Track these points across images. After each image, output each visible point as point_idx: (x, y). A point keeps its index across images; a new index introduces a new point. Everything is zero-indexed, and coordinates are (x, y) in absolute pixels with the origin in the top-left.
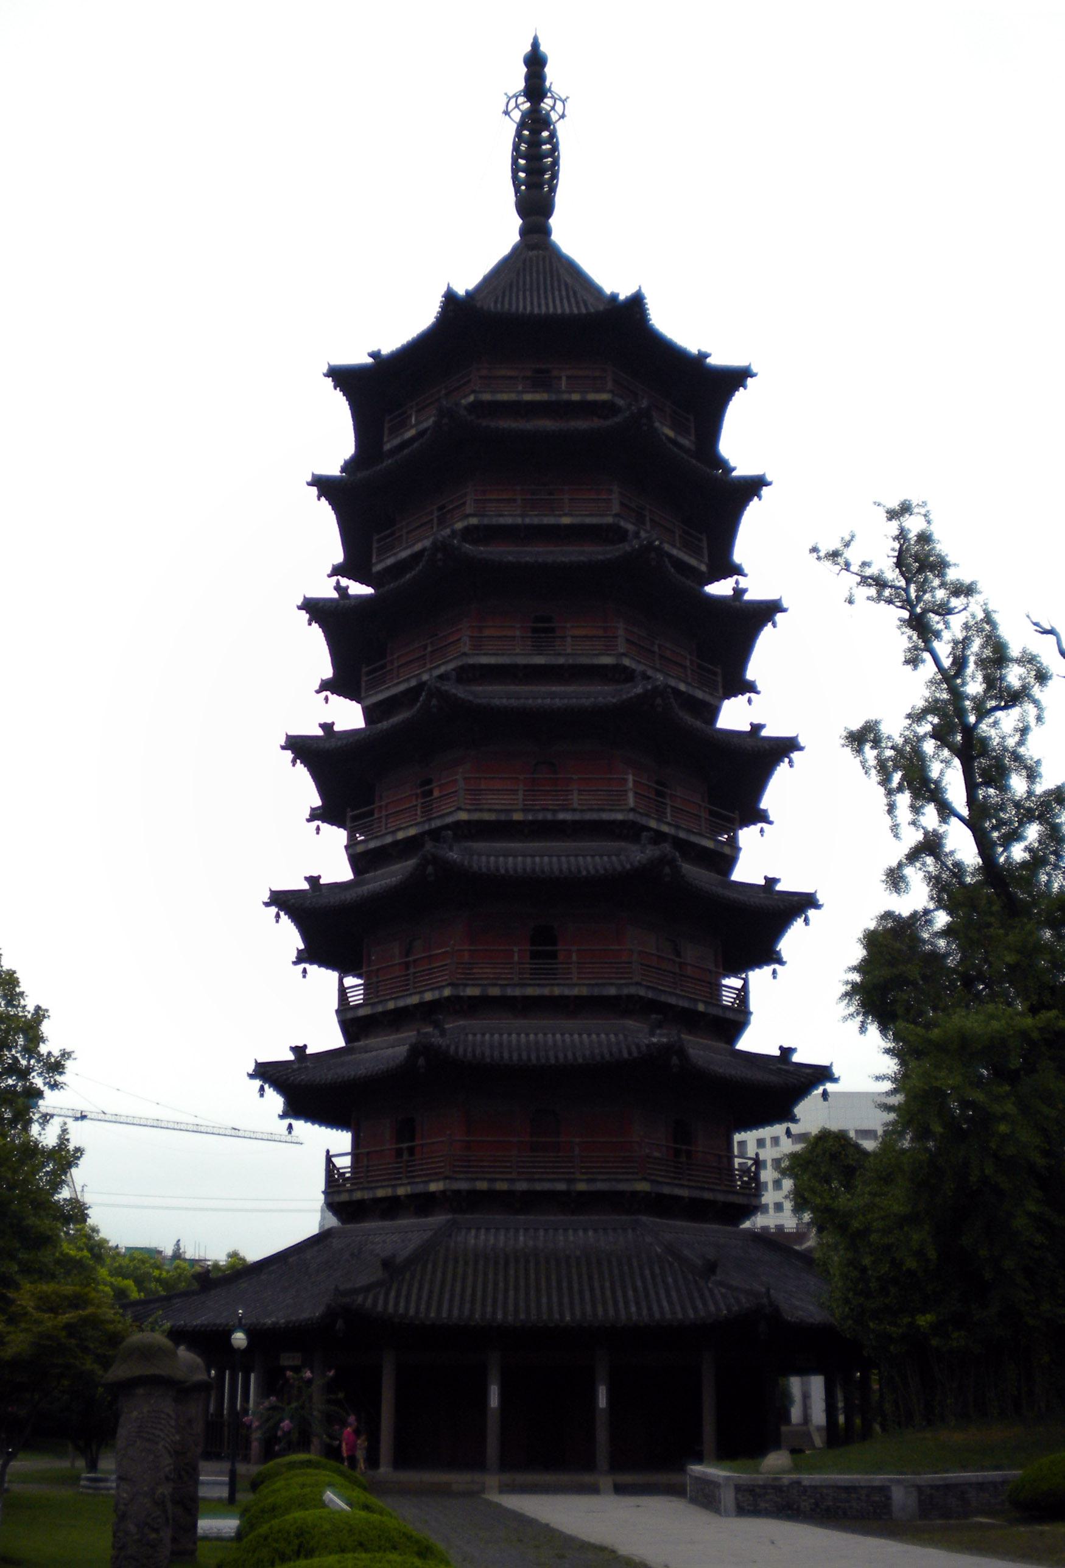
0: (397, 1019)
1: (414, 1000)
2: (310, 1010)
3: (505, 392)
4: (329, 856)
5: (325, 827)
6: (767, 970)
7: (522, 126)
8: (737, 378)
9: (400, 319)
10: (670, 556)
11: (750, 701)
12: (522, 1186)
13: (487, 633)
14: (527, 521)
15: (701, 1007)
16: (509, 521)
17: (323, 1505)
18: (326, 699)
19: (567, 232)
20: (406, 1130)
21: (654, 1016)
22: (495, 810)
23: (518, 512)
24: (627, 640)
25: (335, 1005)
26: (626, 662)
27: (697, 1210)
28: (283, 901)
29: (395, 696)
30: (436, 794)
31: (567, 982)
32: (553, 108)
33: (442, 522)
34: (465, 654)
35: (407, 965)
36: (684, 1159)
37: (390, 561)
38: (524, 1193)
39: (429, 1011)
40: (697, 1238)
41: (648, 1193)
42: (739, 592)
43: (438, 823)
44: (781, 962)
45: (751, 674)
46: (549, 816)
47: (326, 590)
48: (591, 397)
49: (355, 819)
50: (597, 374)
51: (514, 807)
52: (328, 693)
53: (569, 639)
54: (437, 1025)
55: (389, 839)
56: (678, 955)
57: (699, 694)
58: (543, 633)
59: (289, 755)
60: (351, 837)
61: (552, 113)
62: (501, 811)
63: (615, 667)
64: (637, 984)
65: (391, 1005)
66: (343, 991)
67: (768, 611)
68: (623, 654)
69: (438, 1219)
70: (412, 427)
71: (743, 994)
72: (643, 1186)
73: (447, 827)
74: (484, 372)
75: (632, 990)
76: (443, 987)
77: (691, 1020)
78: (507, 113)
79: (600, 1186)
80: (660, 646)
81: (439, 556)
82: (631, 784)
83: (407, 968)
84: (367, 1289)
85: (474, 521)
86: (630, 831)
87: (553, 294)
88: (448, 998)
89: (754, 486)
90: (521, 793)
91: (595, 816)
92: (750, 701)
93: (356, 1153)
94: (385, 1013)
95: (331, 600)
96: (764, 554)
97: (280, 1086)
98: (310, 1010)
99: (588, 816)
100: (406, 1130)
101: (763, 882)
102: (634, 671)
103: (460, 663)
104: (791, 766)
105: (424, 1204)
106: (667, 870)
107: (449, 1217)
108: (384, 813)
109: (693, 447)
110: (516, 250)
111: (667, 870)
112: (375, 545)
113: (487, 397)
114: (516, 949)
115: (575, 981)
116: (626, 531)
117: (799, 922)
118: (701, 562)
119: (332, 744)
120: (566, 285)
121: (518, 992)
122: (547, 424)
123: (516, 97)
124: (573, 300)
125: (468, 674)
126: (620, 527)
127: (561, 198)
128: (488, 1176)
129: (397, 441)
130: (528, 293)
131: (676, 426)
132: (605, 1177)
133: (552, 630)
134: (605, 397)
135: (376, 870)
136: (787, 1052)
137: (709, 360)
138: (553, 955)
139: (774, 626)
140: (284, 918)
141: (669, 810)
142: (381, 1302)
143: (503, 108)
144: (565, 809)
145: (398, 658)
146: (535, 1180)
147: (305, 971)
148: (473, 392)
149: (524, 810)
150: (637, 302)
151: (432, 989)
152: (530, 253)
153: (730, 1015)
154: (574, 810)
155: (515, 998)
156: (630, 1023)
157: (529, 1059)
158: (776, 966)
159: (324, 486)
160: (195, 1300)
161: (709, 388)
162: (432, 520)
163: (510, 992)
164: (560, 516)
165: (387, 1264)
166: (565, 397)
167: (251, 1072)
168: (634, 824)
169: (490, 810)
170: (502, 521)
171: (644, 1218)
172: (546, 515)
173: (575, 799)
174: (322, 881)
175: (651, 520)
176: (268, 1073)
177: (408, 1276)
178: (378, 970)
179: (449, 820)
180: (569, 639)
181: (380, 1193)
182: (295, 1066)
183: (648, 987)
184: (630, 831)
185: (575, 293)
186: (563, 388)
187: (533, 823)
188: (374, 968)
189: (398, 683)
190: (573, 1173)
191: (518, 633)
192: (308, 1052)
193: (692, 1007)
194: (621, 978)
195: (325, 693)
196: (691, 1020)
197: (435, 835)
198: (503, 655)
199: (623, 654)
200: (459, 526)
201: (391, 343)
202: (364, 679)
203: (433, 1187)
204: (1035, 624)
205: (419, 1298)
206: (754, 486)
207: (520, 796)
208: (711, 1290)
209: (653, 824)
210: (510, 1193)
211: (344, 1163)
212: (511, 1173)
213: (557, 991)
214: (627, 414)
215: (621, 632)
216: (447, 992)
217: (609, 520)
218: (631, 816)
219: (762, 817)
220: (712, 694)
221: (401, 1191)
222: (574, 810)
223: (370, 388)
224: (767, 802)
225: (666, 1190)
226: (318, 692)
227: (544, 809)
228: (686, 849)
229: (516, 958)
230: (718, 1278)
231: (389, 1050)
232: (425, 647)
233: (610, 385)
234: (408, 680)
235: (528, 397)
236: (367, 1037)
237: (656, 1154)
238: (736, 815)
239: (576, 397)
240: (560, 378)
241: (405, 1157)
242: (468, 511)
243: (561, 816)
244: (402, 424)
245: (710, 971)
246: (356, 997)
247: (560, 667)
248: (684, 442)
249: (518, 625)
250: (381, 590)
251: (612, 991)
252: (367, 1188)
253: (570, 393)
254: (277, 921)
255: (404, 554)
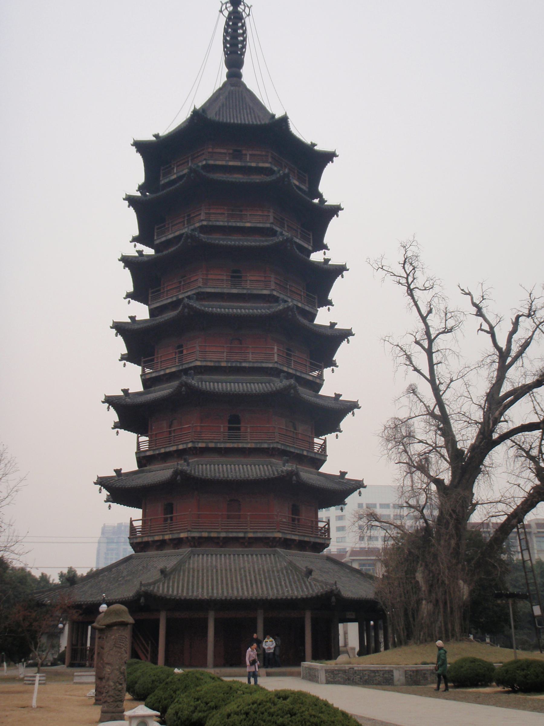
0: (165, 457)
1: (174, 448)
2: (123, 451)
3: (220, 160)
4: (131, 379)
5: (128, 363)
6: (334, 434)
7: (229, 18)
8: (329, 157)
9: (167, 118)
10: (296, 242)
11: (329, 309)
12: (223, 535)
13: (210, 277)
14: (230, 224)
15: (305, 453)
16: (221, 224)
17: (174, 673)
18: (129, 302)
19: (249, 77)
20: (169, 509)
21: (285, 458)
22: (213, 361)
23: (226, 220)
24: (275, 283)
25: (136, 450)
26: (275, 293)
27: (302, 546)
28: (111, 401)
29: (166, 304)
30: (185, 352)
31: (246, 441)
32: (244, 11)
33: (189, 222)
34: (200, 287)
35: (170, 432)
36: (296, 522)
37: (163, 239)
38: (224, 538)
39: (180, 454)
40: (302, 560)
41: (280, 538)
42: (327, 261)
43: (186, 366)
44: (341, 431)
45: (326, 241)
46: (238, 365)
47: (132, 250)
48: (261, 165)
49: (145, 362)
50: (264, 153)
51: (222, 360)
52: (130, 299)
53: (248, 281)
54: (185, 460)
55: (162, 373)
56: (295, 429)
57: (307, 308)
58: (236, 277)
59: (114, 331)
60: (143, 371)
61: (243, 13)
62: (216, 361)
63: (269, 295)
64: (277, 442)
65: (163, 451)
66: (138, 443)
67: (340, 270)
68: (273, 290)
69: (185, 550)
70: (174, 174)
71: (324, 447)
72: (279, 535)
73: (190, 368)
74: (210, 150)
75: (275, 445)
76: (188, 443)
77: (300, 458)
78: (221, 11)
79: (259, 535)
80: (290, 286)
81: (189, 240)
82: (276, 350)
83: (170, 434)
84: (154, 583)
85: (205, 223)
86: (275, 372)
87: (243, 111)
88: (190, 448)
89: (335, 210)
90: (225, 354)
91: (259, 365)
92: (329, 309)
93: (144, 520)
94: (159, 454)
95: (135, 257)
96: (338, 243)
97: (107, 488)
98: (123, 451)
99: (256, 365)
100: (169, 509)
101: (334, 396)
102: (278, 297)
103: (197, 291)
104: (348, 343)
105: (178, 543)
106: (292, 391)
107: (190, 549)
108: (159, 360)
109: (307, 190)
110: (225, 85)
111: (292, 391)
112: (156, 231)
113: (211, 162)
114: (222, 426)
115: (249, 441)
116: (277, 231)
117: (345, 343)
118: (309, 245)
119: (136, 327)
120: (249, 106)
121: (222, 446)
122: (238, 177)
123: (226, 3)
124: (253, 115)
125: (201, 296)
126: (273, 229)
127: (247, 59)
128: (208, 530)
129: (166, 180)
130: (231, 110)
131: (300, 180)
132: (261, 530)
133: (240, 277)
134: (267, 165)
135: (155, 386)
136: (343, 474)
137: (316, 148)
138: (239, 429)
139: (342, 277)
140: (111, 408)
141: (292, 362)
142: (161, 588)
143: (220, 9)
144: (245, 361)
145: (167, 286)
146: (229, 532)
147: (118, 432)
148: (205, 159)
149: (226, 361)
150: (284, 120)
151: (183, 444)
152: (232, 88)
153: (318, 457)
154: (250, 362)
155: (221, 448)
156: (274, 460)
157: (228, 477)
158: (338, 433)
159: (131, 201)
160: (56, 585)
161: (314, 161)
162: (184, 221)
163: (219, 445)
164: (245, 222)
165: (163, 572)
166: (249, 164)
167: (95, 481)
168: (277, 369)
169: (211, 361)
170: (218, 224)
171: (278, 549)
172: (238, 222)
173: (250, 357)
174: (130, 392)
175: (287, 225)
176: (102, 482)
177: (172, 576)
178: (156, 434)
179: (192, 365)
180: (248, 281)
181: (156, 538)
182: (116, 479)
183: (282, 444)
184: (275, 372)
185: (254, 111)
186: (248, 160)
187: (230, 367)
188: (154, 433)
189: (167, 299)
190: (247, 529)
191: (225, 278)
192: (122, 472)
193: (301, 453)
194: (269, 440)
195: (128, 299)
196: (300, 458)
197: (186, 372)
198: (218, 288)
199: (273, 290)
200: (197, 225)
201: (163, 132)
202: (150, 295)
203: (182, 535)
204: (463, 290)
205: (178, 587)
206: (335, 210)
207: (225, 354)
208: (310, 583)
209: (285, 369)
210: (218, 538)
211: (138, 524)
212: (218, 529)
213: (241, 445)
214: (278, 175)
215: (273, 279)
216: (190, 445)
217: (268, 225)
218: (276, 365)
219: (334, 364)
220: (312, 308)
221: (167, 537)
222: (250, 362)
223: (153, 152)
224: (337, 357)
225: (288, 537)
226: (125, 298)
227: (235, 361)
228: (299, 379)
229: (222, 430)
230: (313, 577)
231: (161, 473)
232: (180, 282)
233: (270, 160)
234: (172, 297)
235: (231, 163)
236: (150, 464)
237: (284, 520)
238: (322, 365)
239: (254, 165)
240: (246, 155)
241: (169, 521)
242: (202, 218)
243: (244, 365)
244: (169, 172)
245: (309, 437)
246: (145, 447)
247: (244, 294)
248: (303, 187)
249: (225, 274)
250: (160, 254)
251: (266, 446)
252: (150, 536)
253: (251, 162)
254: (108, 410)
255: (171, 236)
